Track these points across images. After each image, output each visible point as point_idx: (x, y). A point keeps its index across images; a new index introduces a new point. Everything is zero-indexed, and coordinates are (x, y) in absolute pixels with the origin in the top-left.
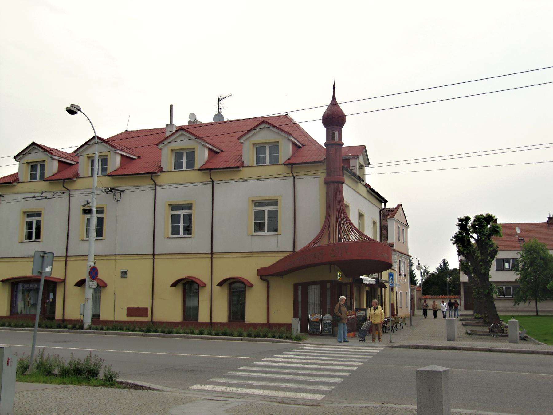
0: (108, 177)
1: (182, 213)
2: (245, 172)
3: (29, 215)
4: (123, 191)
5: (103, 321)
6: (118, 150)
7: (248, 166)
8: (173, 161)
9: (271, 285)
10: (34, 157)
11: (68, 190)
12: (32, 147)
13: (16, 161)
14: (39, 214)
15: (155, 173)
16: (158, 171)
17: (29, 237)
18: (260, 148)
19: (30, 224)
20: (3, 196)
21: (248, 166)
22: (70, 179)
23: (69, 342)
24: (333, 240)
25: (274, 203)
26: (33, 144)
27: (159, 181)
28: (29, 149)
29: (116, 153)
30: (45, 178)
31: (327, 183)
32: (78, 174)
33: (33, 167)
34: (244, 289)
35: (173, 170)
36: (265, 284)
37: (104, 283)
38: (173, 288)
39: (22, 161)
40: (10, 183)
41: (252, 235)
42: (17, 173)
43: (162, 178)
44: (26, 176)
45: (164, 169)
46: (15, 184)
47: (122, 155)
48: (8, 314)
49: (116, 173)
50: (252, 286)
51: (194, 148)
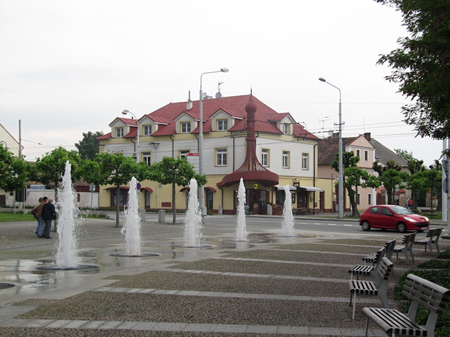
0: (153, 137)
1: (222, 153)
2: (213, 134)
3: (220, 150)
4: (159, 144)
5: (152, 209)
6: (233, 116)
7: (214, 131)
8: (218, 126)
9: (224, 191)
10: (119, 124)
11: (134, 142)
12: (117, 120)
13: (110, 127)
14: (149, 153)
15: (172, 135)
16: (109, 138)
17: (220, 162)
18: (220, 122)
19: (219, 156)
20: (105, 145)
21: (214, 131)
22: (208, 132)
23: (448, 219)
24: (247, 170)
25: (225, 150)
26: (117, 118)
27: (174, 138)
28: (116, 121)
29: (194, 120)
30: (124, 136)
31: (248, 140)
32: (176, 132)
33: (118, 130)
34: (208, 192)
35: (144, 135)
36: (221, 190)
37: (151, 190)
38: (181, 193)
39: (113, 127)
40: (107, 139)
41: (216, 166)
42: (111, 133)
43: (177, 137)
44: (114, 135)
45: (177, 132)
46: (110, 139)
47: (235, 119)
48: (110, 206)
49: (156, 134)
50: (215, 191)
51: (190, 122)
